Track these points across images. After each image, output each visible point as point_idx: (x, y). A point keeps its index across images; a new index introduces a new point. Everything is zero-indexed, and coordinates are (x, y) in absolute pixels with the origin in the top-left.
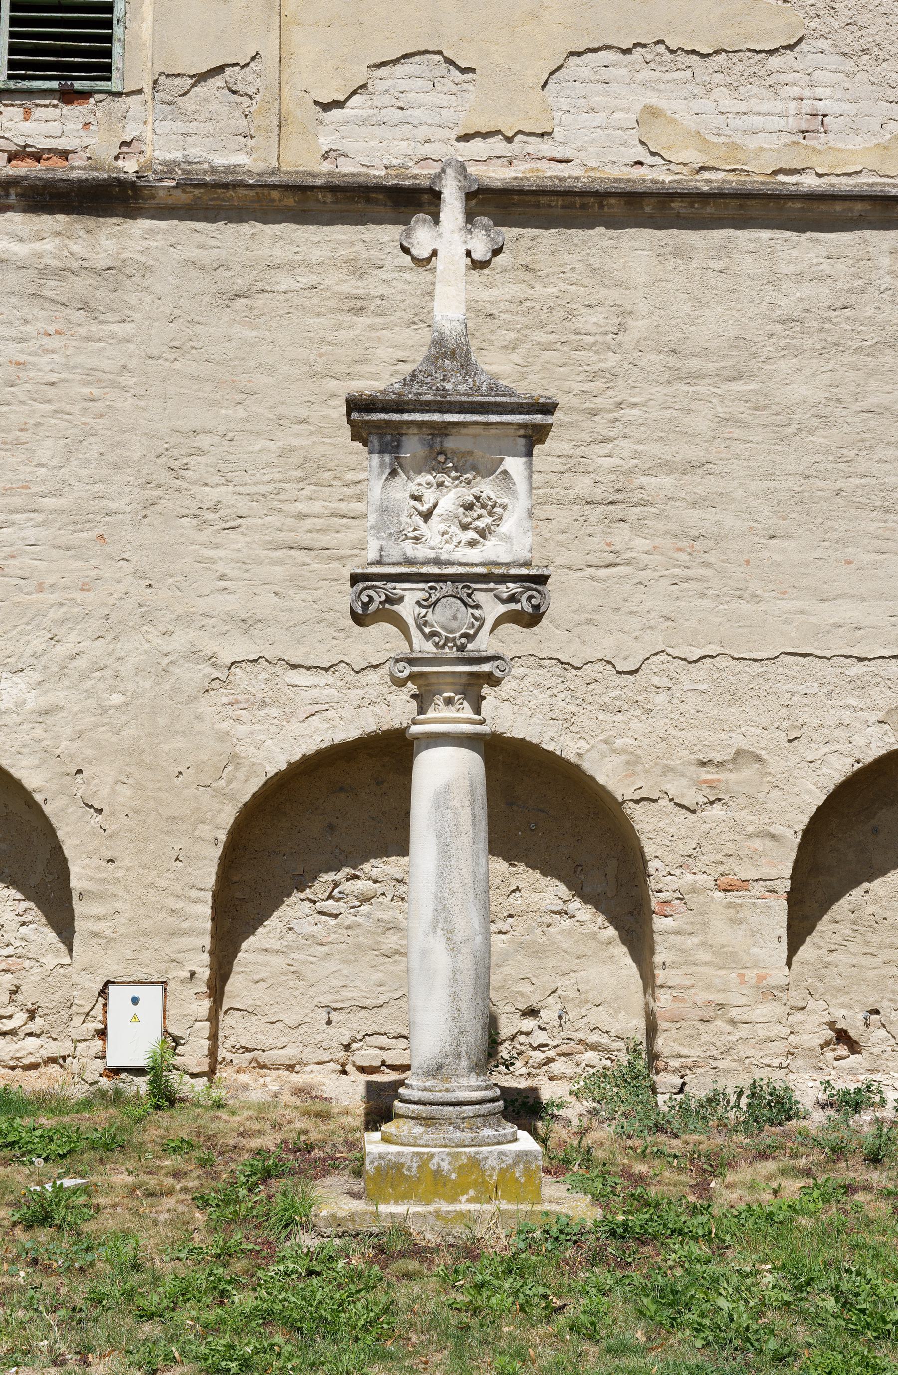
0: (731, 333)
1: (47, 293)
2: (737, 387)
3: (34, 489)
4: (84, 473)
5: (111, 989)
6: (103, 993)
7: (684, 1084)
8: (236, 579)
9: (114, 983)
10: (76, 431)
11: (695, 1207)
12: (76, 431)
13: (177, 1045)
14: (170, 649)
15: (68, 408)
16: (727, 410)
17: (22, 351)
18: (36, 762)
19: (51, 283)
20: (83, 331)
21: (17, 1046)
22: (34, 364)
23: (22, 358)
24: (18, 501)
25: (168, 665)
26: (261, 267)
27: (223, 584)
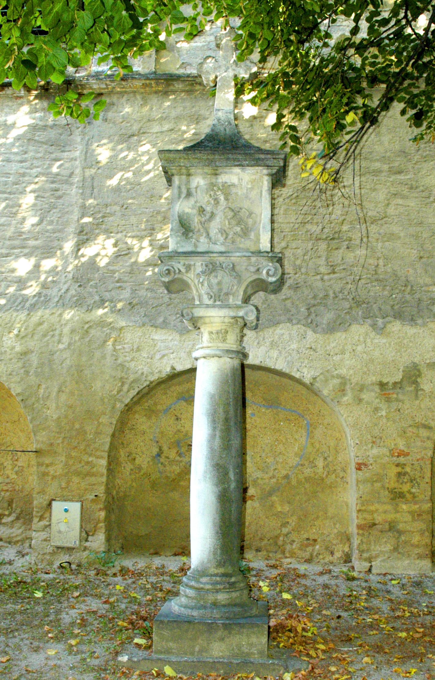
0: (397, 147)
1: (37, 138)
2: (402, 177)
3: (24, 236)
4: (49, 227)
5: (54, 504)
6: (50, 505)
7: (371, 566)
8: (126, 282)
9: (55, 500)
10: (47, 206)
11: (285, 74)
12: (47, 206)
13: (88, 535)
14: (89, 319)
15: (43, 194)
16: (395, 189)
17: (22, 167)
18: (19, 380)
19: (39, 133)
20: (53, 156)
21: (11, 531)
22: (28, 173)
23: (22, 171)
24: (17, 242)
25: (88, 328)
26: (145, 120)
27: (118, 284)
